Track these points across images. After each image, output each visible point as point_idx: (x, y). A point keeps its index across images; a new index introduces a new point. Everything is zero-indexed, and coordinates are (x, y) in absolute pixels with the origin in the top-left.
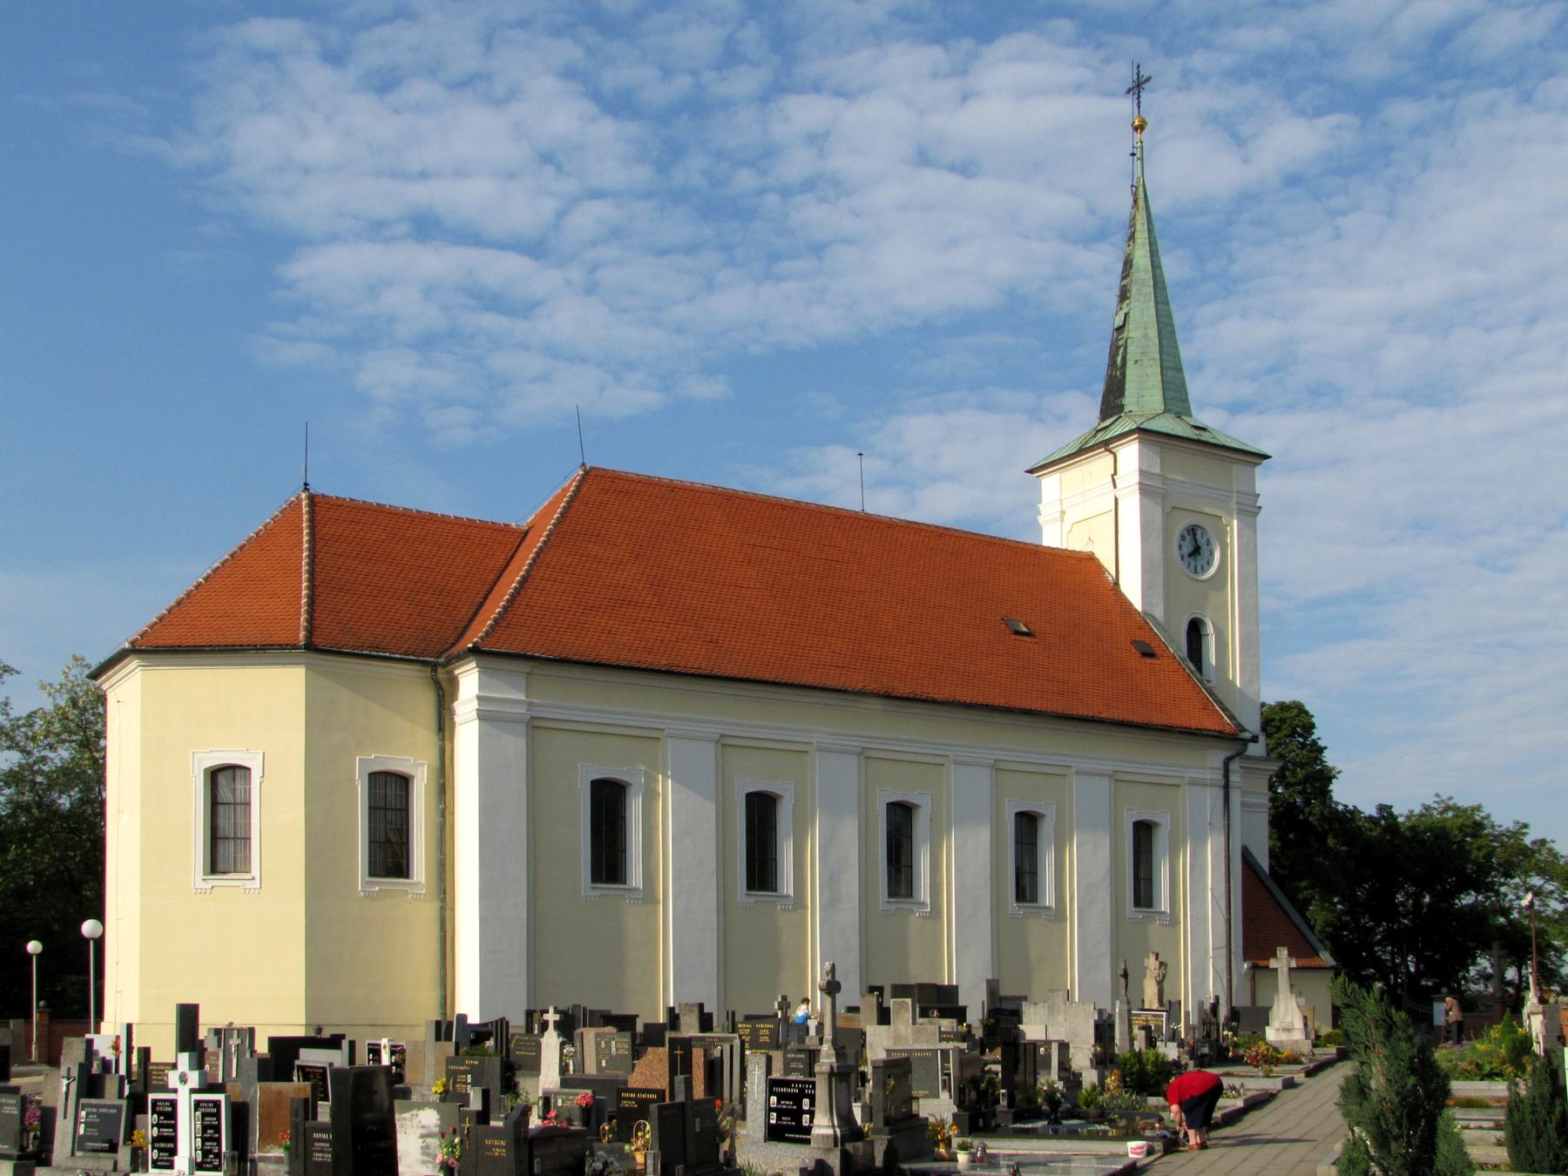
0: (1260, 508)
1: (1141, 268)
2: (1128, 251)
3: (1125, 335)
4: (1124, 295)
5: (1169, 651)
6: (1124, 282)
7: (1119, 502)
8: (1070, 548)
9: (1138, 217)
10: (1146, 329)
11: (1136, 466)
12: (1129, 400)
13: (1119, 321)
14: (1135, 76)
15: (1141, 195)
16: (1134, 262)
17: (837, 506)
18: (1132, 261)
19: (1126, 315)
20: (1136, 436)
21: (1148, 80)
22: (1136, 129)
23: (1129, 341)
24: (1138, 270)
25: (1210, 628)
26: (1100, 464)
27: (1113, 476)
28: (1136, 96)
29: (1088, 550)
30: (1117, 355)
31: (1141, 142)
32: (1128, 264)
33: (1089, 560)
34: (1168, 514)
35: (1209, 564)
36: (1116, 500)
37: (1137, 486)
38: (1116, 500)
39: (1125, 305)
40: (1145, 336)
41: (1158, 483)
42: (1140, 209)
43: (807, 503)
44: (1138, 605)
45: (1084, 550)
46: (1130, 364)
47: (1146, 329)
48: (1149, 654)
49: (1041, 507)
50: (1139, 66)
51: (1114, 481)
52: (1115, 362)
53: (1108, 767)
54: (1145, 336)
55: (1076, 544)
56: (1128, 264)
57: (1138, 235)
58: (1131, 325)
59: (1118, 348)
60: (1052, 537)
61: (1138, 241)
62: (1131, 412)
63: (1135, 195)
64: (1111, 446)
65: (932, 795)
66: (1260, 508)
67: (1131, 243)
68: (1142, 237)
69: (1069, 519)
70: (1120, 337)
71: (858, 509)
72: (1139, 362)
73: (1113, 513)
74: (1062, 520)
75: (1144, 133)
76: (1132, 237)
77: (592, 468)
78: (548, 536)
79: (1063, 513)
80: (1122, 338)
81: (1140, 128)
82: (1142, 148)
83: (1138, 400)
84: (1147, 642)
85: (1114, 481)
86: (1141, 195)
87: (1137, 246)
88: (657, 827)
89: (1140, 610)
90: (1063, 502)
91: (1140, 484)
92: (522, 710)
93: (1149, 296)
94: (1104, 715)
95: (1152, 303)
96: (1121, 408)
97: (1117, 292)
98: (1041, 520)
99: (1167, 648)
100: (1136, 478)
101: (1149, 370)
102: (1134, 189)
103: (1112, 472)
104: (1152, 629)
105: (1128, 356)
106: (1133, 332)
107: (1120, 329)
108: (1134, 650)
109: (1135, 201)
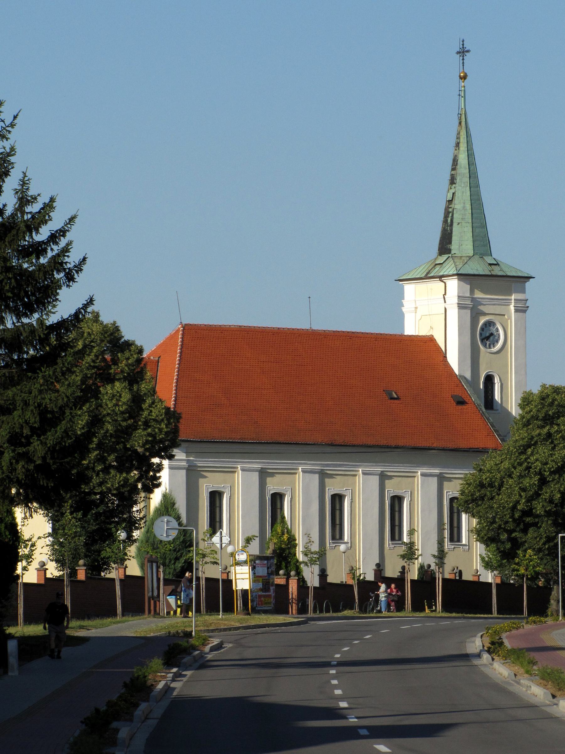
0: (528, 307)
1: (463, 166)
2: (455, 154)
3: (452, 206)
4: (452, 181)
5: (472, 400)
6: (453, 172)
7: (447, 310)
8: (420, 334)
9: (462, 133)
10: (464, 203)
11: (456, 294)
12: (454, 247)
13: (450, 197)
14: (461, 46)
15: (463, 120)
16: (459, 162)
17: (298, 328)
18: (457, 161)
19: (453, 194)
20: (456, 277)
21: (468, 51)
22: (461, 78)
23: (455, 212)
24: (461, 167)
25: (497, 380)
26: (437, 285)
27: (444, 295)
28: (461, 58)
29: (430, 334)
30: (448, 217)
31: (464, 87)
32: (455, 161)
33: (431, 340)
34: (474, 317)
35: (497, 341)
36: (445, 309)
37: (457, 305)
38: (445, 309)
39: (453, 187)
40: (464, 208)
41: (468, 302)
42: (463, 128)
43: (283, 328)
44: (457, 371)
45: (428, 334)
46: (455, 225)
47: (464, 203)
48: (461, 402)
49: (404, 302)
50: (463, 41)
51: (444, 298)
52: (447, 221)
53: (437, 471)
54: (464, 208)
55: (423, 332)
56: (455, 161)
57: (461, 145)
58: (456, 201)
59: (449, 212)
60: (410, 330)
61: (461, 149)
62: (455, 254)
63: (460, 119)
64: (443, 279)
65: (352, 490)
66: (528, 307)
67: (457, 149)
68: (463, 147)
69: (420, 312)
70: (450, 206)
71: (308, 327)
72: (460, 224)
73: (444, 314)
74: (416, 312)
75: (466, 81)
76: (458, 145)
77: (185, 325)
78: (178, 372)
79: (416, 308)
80: (451, 208)
81: (464, 78)
82: (465, 90)
83: (459, 247)
84: (460, 395)
85: (444, 298)
86: (463, 120)
87: (460, 151)
88: (235, 511)
89: (457, 373)
90: (416, 302)
91: (458, 304)
92: (184, 464)
93: (466, 183)
94: (435, 445)
95: (468, 188)
96: (449, 251)
97: (449, 178)
98: (404, 309)
99: (471, 398)
100: (456, 300)
101: (466, 229)
102: (459, 115)
103: (444, 293)
104: (463, 386)
105: (454, 220)
106: (457, 205)
107: (450, 202)
108: (452, 401)
109: (460, 123)
